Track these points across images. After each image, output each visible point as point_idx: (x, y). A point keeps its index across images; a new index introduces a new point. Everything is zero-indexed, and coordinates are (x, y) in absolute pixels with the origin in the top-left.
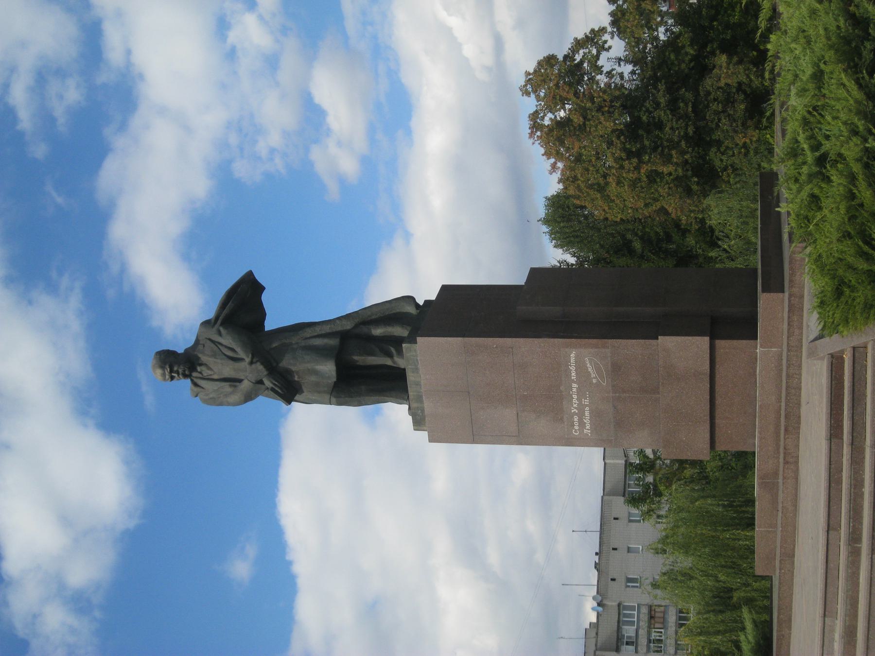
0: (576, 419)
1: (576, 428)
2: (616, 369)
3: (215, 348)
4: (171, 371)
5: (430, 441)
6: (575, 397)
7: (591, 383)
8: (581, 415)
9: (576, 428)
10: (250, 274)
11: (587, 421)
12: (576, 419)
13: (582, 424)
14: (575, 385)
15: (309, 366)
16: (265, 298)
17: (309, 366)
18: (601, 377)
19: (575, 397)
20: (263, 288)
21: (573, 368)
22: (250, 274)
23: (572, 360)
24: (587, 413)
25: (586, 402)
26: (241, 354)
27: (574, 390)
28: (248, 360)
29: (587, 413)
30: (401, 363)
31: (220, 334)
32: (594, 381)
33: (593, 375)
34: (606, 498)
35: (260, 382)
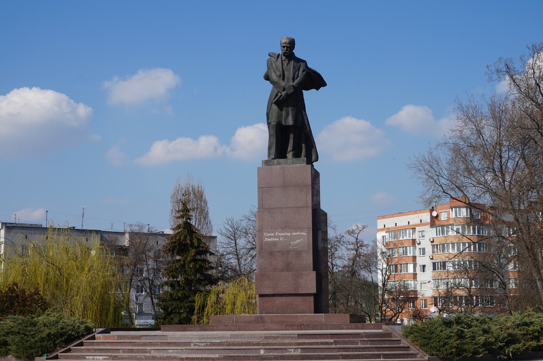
0: (273, 234)
1: (268, 235)
2: (298, 253)
3: (297, 68)
4: (287, 47)
5: (258, 168)
6: (284, 234)
7: (291, 242)
8: (274, 237)
9: (268, 235)
10: (324, 84)
11: (272, 239)
12: (273, 234)
13: (270, 237)
14: (289, 234)
15: (290, 113)
16: (314, 90)
17: (290, 113)
18: (294, 246)
19: (284, 234)
20: (317, 90)
21: (298, 233)
22: (324, 84)
23: (302, 233)
24: (275, 239)
25: (281, 239)
26: (296, 82)
27: (287, 234)
28: (294, 84)
29: (275, 239)
30: (290, 155)
31: (303, 71)
32: (292, 243)
33: (294, 242)
34: (95, 241)
35: (284, 90)
